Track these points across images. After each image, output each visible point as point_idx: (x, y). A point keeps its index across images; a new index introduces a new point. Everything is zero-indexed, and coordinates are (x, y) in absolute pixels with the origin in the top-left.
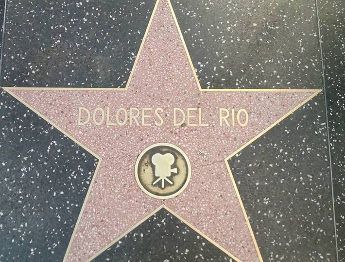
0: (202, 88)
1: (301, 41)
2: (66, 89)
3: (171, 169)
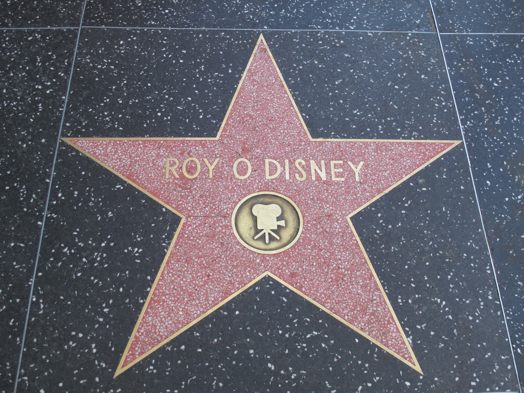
3: (277, 221)
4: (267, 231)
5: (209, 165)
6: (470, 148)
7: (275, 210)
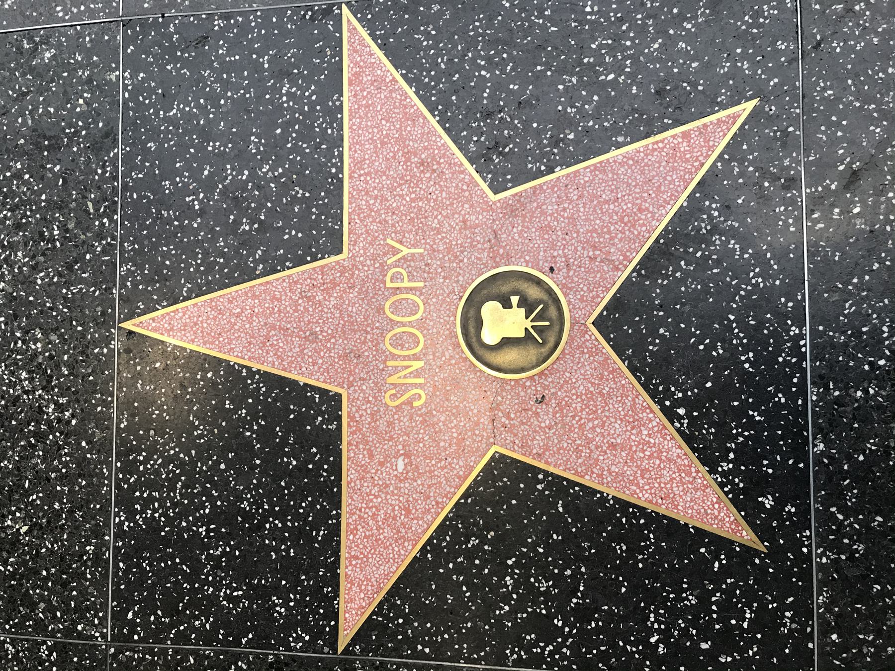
0: (495, 194)
1: (435, 9)
2: (551, 469)
3: (511, 307)
4: (528, 324)
5: (399, 256)
6: (822, 653)
7: (490, 310)
